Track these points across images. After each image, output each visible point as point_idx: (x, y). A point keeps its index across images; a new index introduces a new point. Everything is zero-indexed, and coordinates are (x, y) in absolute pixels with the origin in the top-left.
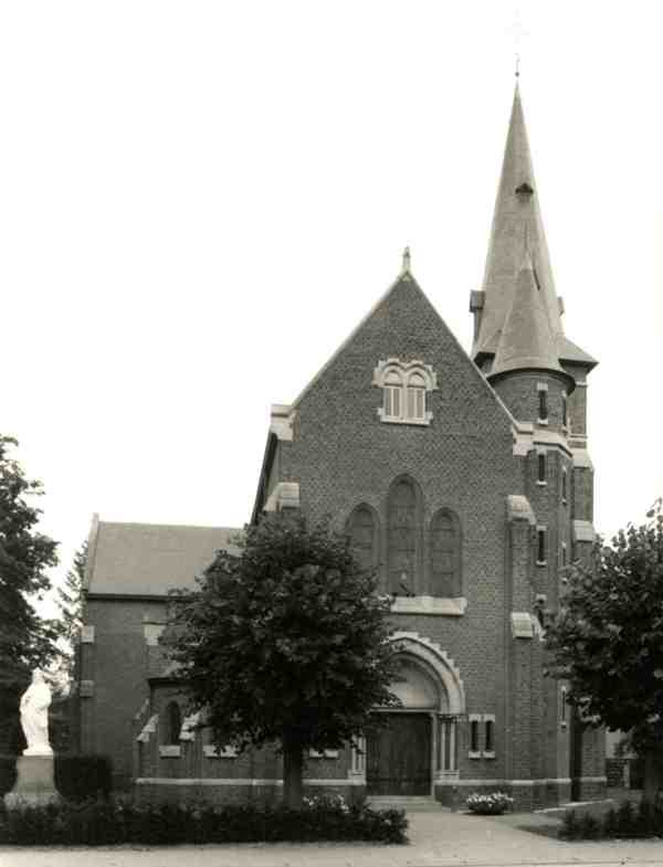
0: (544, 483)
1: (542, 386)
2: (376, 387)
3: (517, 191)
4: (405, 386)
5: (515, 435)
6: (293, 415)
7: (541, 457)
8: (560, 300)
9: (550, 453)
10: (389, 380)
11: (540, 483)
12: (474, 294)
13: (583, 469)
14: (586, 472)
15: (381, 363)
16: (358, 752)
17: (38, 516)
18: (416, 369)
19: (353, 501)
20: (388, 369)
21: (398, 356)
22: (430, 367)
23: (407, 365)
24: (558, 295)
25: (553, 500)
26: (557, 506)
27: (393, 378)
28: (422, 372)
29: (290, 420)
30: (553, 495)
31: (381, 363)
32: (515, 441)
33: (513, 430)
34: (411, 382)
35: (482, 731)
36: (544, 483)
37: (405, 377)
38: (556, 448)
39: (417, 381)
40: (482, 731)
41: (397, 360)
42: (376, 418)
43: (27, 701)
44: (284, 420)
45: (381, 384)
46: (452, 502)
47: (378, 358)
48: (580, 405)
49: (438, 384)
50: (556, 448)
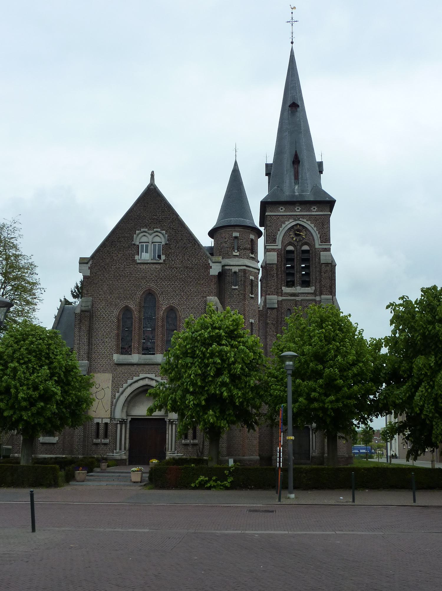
0: (237, 287)
1: (236, 234)
2: (134, 245)
3: (290, 106)
4: (150, 243)
5: (211, 264)
6: (90, 262)
7: (235, 273)
8: (320, 164)
9: (240, 270)
10: (142, 240)
11: (233, 287)
12: (267, 165)
13: (327, 264)
14: (331, 266)
15: (137, 232)
16: (182, 456)
17: (37, 310)
18: (157, 233)
19: (122, 305)
20: (142, 234)
21: (147, 228)
22: (164, 232)
23: (151, 232)
24: (318, 159)
25: (242, 297)
26: (244, 299)
27: (144, 239)
28: (159, 234)
29: (89, 265)
30: (242, 294)
31: (137, 232)
32: (211, 267)
33: (210, 262)
34: (154, 241)
35: (102, 428)
36: (237, 287)
37: (150, 238)
38: (245, 267)
39: (157, 239)
40: (102, 428)
41: (146, 230)
42: (134, 261)
43: (377, 465)
44: (85, 265)
45: (137, 243)
46: (174, 302)
47: (136, 229)
48: (325, 227)
49: (168, 240)
50: (245, 267)
